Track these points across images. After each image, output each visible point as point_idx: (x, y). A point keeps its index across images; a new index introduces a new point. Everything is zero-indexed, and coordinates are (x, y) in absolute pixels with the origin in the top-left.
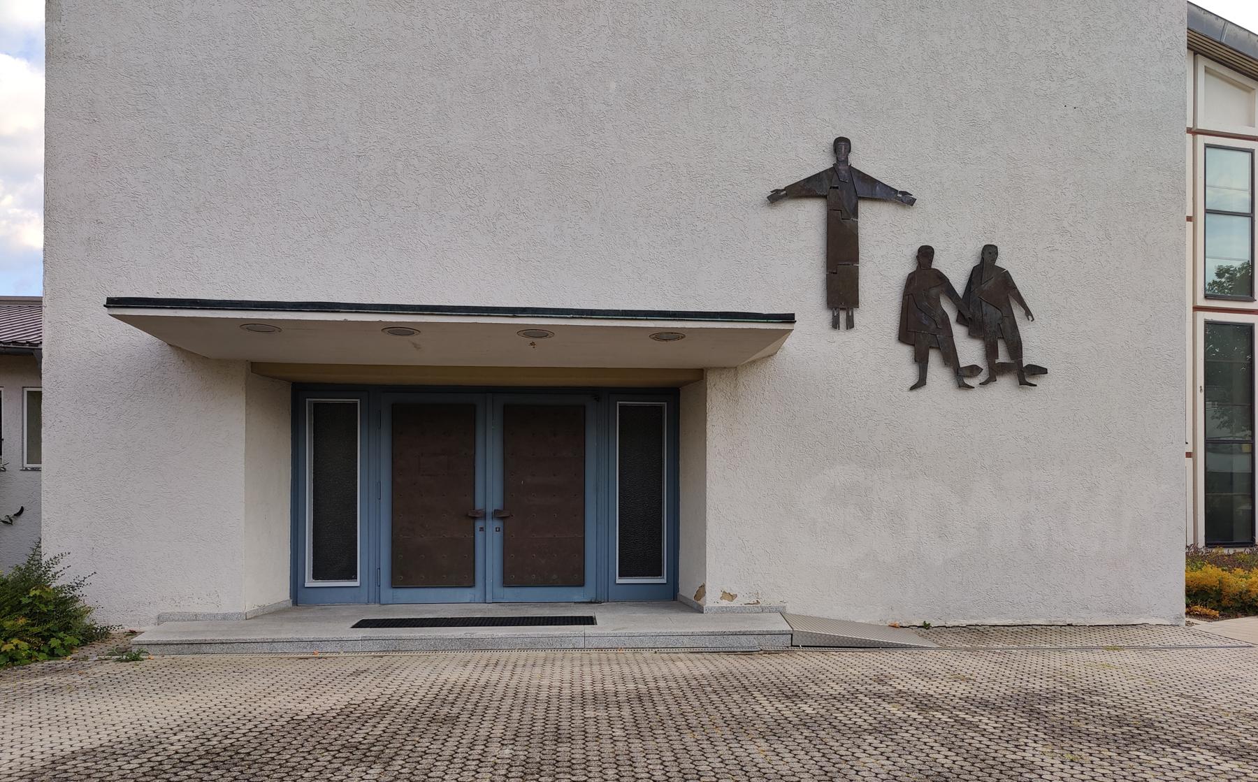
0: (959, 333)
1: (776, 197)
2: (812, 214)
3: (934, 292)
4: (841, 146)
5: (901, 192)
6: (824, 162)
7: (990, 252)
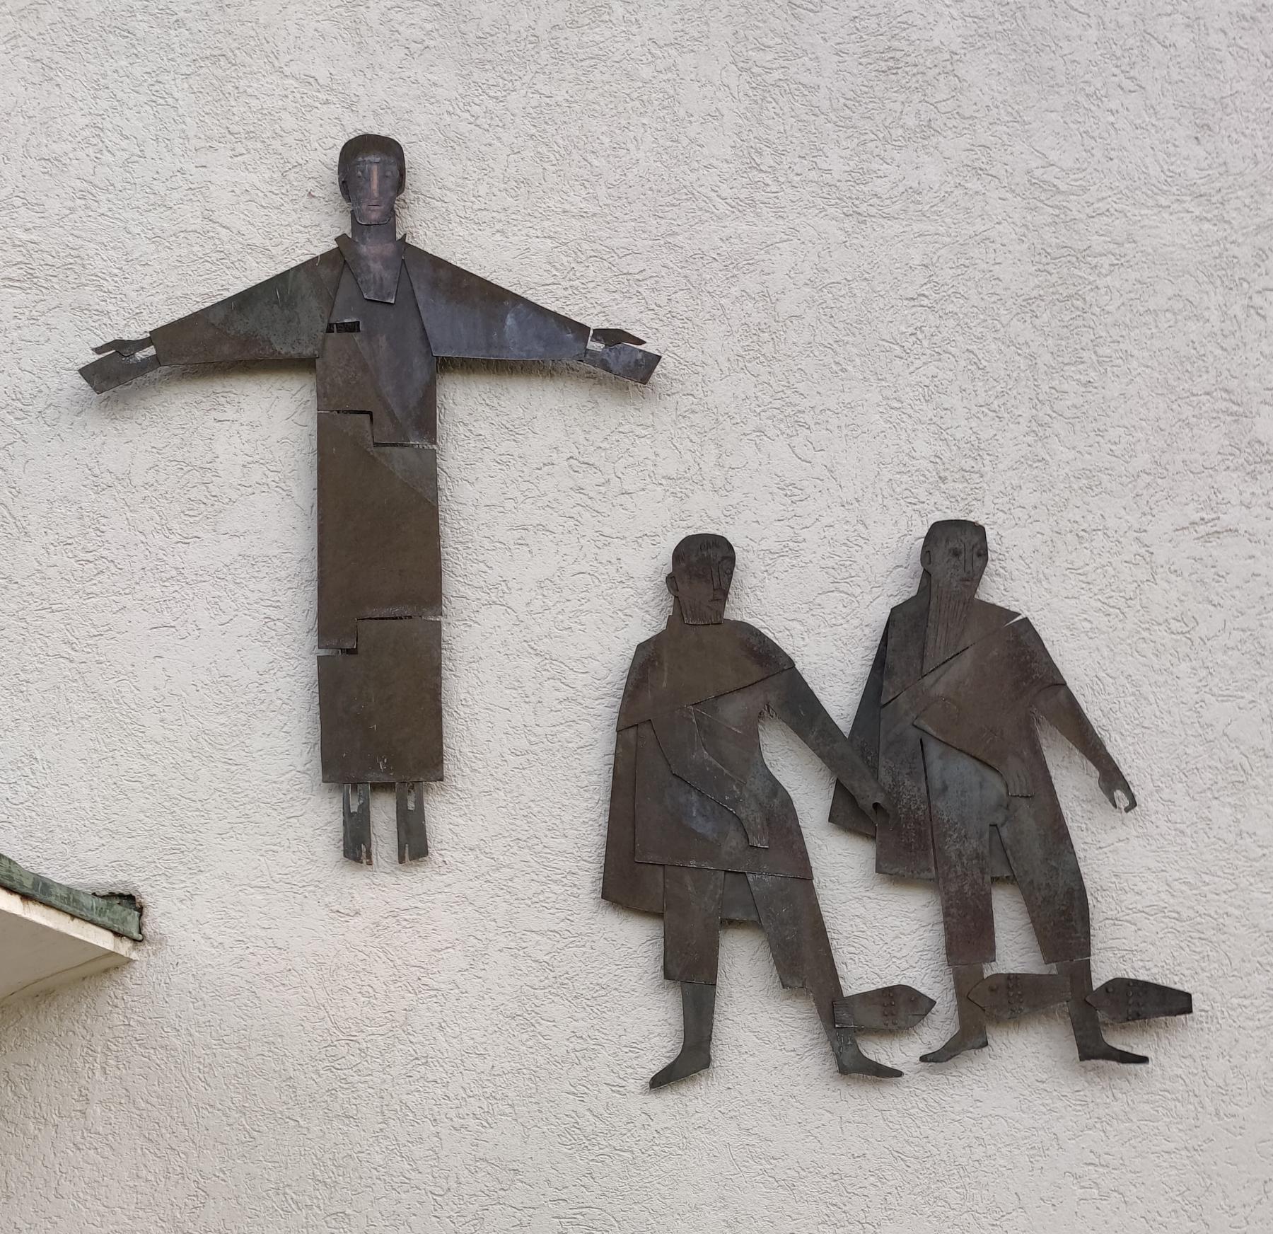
0: (840, 866)
1: (116, 372)
2: (261, 434)
3: (733, 711)
4: (371, 168)
5: (602, 334)
6: (303, 229)
7: (955, 548)
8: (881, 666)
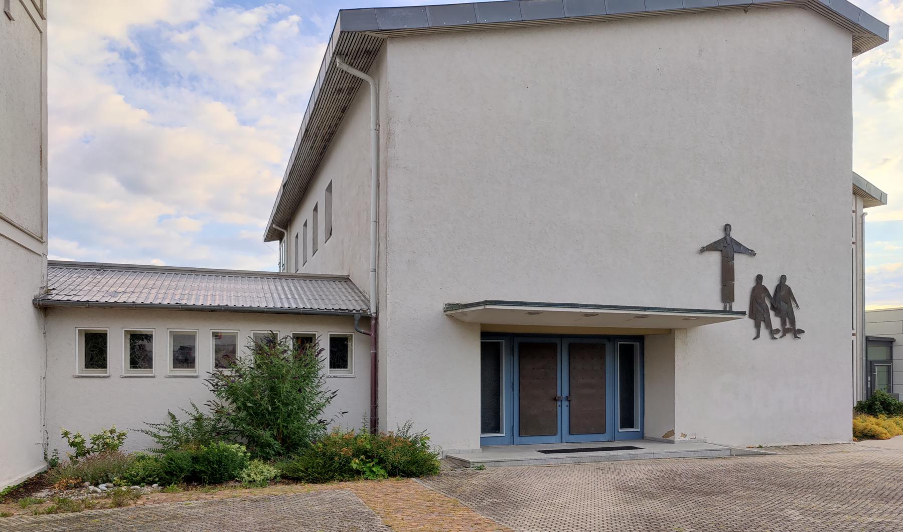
1: (703, 250)
4: (727, 228)
6: (720, 235)
7: (783, 278)
8: (776, 291)
